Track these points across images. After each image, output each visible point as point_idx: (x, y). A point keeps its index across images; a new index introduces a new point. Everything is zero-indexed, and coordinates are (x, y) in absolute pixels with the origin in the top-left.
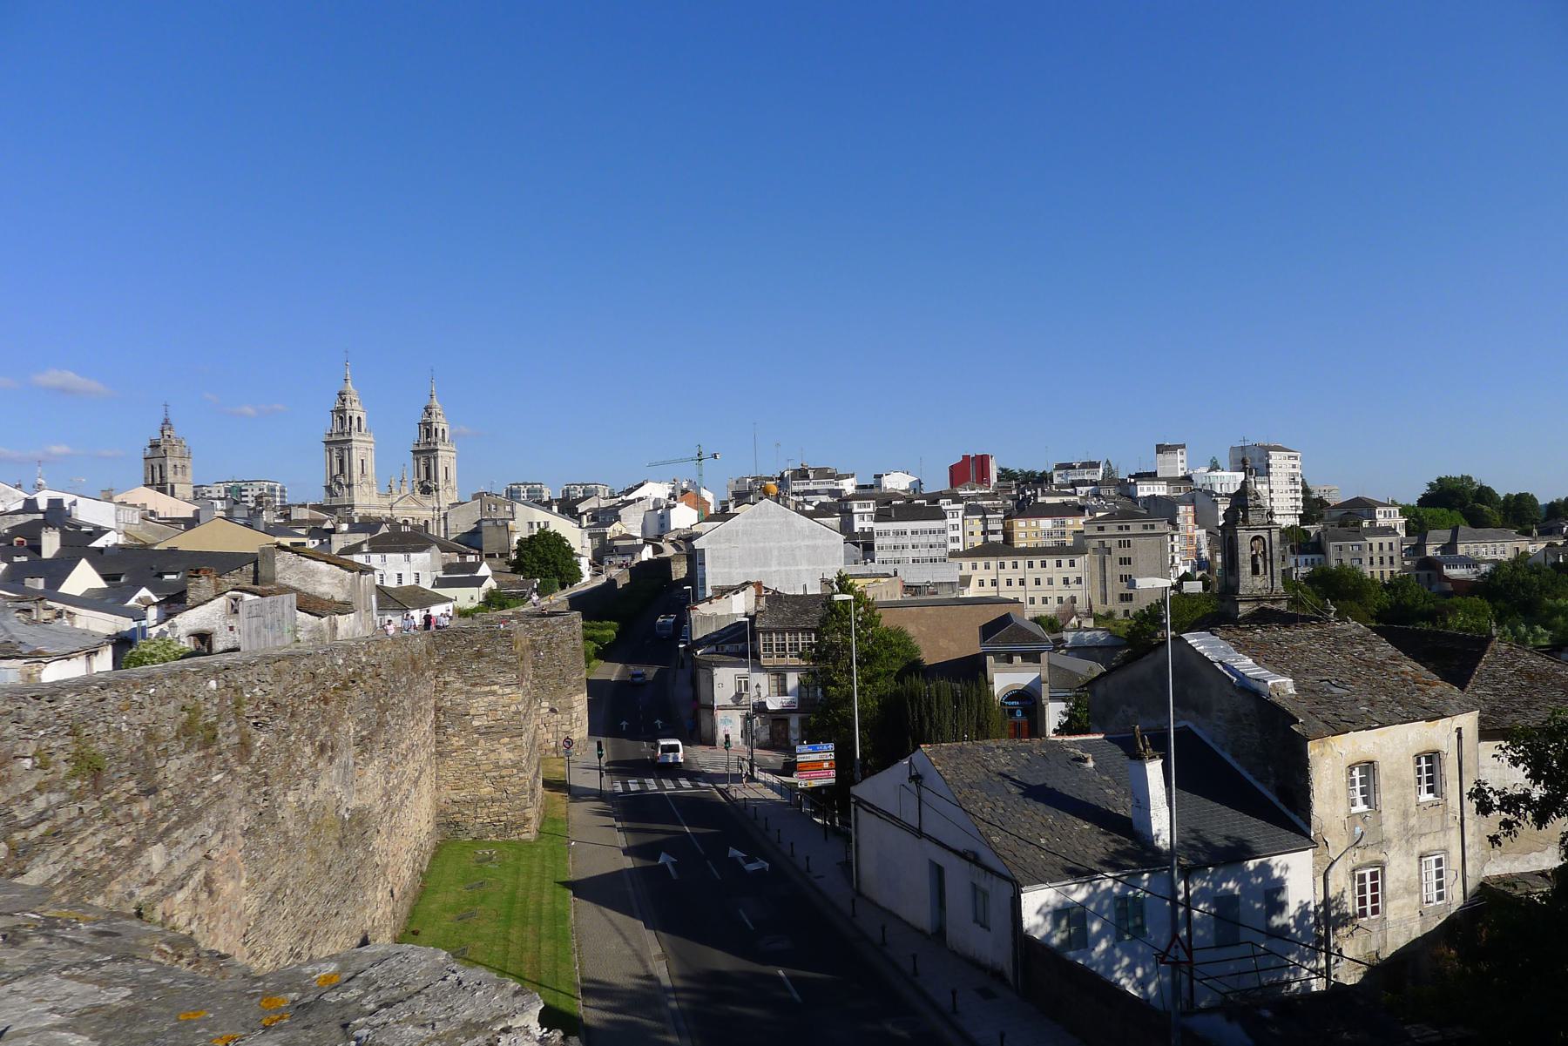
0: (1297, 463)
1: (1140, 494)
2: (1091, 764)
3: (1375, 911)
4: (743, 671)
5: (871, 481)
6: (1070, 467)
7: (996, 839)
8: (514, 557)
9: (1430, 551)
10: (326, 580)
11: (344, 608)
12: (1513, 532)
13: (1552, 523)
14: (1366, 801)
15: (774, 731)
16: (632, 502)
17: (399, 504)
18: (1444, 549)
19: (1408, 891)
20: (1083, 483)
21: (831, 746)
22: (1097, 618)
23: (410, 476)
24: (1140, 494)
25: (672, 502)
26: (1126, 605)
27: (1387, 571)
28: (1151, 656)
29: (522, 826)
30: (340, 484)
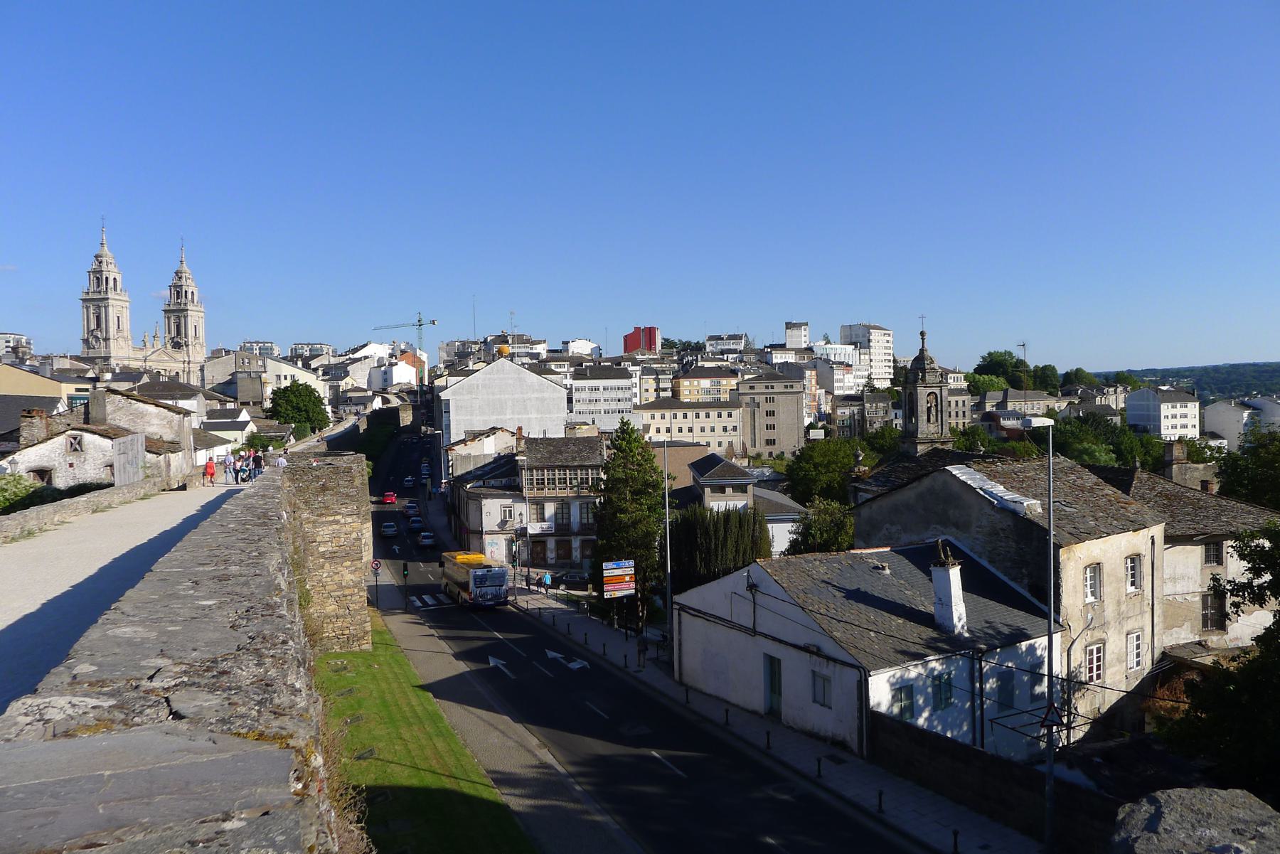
0: (890, 339)
1: (775, 361)
2: (888, 571)
3: (1098, 677)
4: (509, 502)
5: (559, 347)
6: (719, 338)
7: (838, 635)
8: (268, 404)
9: (989, 407)
10: (155, 421)
11: (174, 447)
12: (1045, 393)
13: (1068, 387)
14: (1093, 594)
15: (532, 550)
16: (359, 360)
17: (153, 357)
18: (999, 406)
19: (1119, 661)
20: (734, 351)
21: (632, 563)
22: (750, 458)
23: (162, 332)
24: (775, 361)
25: (394, 360)
26: (770, 448)
27: (960, 422)
28: (915, 484)
29: (363, 638)
30: (97, 338)
